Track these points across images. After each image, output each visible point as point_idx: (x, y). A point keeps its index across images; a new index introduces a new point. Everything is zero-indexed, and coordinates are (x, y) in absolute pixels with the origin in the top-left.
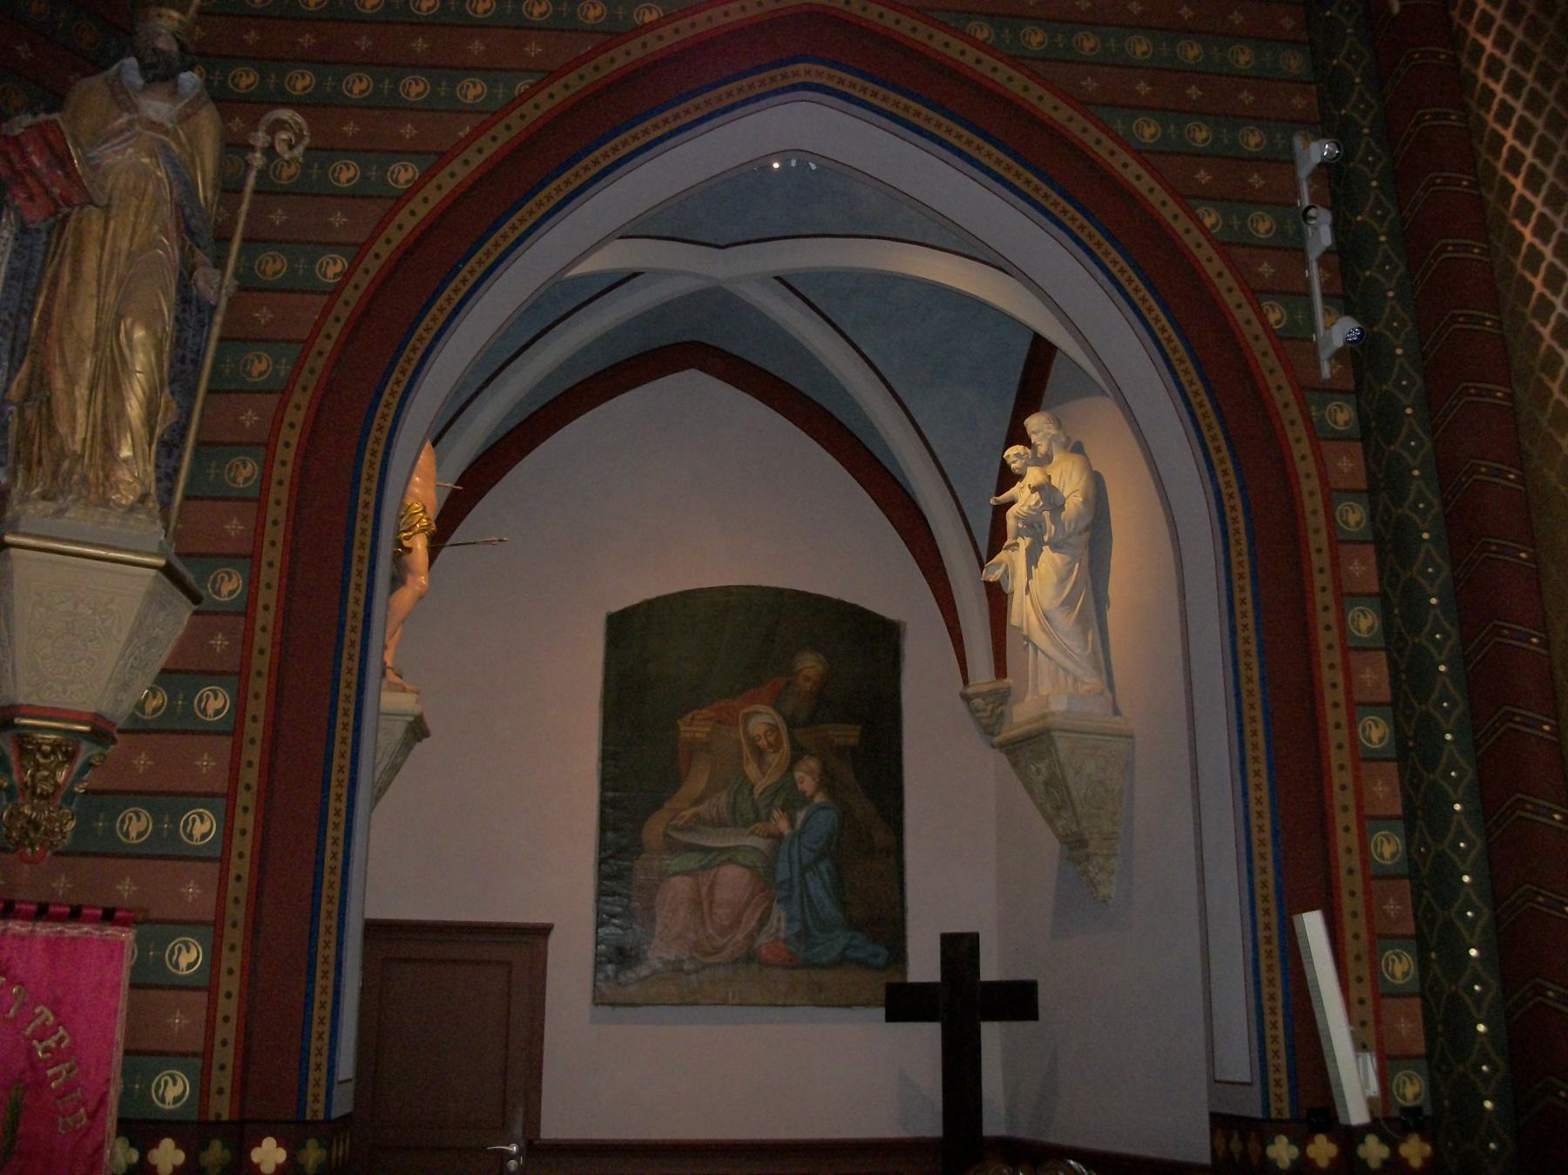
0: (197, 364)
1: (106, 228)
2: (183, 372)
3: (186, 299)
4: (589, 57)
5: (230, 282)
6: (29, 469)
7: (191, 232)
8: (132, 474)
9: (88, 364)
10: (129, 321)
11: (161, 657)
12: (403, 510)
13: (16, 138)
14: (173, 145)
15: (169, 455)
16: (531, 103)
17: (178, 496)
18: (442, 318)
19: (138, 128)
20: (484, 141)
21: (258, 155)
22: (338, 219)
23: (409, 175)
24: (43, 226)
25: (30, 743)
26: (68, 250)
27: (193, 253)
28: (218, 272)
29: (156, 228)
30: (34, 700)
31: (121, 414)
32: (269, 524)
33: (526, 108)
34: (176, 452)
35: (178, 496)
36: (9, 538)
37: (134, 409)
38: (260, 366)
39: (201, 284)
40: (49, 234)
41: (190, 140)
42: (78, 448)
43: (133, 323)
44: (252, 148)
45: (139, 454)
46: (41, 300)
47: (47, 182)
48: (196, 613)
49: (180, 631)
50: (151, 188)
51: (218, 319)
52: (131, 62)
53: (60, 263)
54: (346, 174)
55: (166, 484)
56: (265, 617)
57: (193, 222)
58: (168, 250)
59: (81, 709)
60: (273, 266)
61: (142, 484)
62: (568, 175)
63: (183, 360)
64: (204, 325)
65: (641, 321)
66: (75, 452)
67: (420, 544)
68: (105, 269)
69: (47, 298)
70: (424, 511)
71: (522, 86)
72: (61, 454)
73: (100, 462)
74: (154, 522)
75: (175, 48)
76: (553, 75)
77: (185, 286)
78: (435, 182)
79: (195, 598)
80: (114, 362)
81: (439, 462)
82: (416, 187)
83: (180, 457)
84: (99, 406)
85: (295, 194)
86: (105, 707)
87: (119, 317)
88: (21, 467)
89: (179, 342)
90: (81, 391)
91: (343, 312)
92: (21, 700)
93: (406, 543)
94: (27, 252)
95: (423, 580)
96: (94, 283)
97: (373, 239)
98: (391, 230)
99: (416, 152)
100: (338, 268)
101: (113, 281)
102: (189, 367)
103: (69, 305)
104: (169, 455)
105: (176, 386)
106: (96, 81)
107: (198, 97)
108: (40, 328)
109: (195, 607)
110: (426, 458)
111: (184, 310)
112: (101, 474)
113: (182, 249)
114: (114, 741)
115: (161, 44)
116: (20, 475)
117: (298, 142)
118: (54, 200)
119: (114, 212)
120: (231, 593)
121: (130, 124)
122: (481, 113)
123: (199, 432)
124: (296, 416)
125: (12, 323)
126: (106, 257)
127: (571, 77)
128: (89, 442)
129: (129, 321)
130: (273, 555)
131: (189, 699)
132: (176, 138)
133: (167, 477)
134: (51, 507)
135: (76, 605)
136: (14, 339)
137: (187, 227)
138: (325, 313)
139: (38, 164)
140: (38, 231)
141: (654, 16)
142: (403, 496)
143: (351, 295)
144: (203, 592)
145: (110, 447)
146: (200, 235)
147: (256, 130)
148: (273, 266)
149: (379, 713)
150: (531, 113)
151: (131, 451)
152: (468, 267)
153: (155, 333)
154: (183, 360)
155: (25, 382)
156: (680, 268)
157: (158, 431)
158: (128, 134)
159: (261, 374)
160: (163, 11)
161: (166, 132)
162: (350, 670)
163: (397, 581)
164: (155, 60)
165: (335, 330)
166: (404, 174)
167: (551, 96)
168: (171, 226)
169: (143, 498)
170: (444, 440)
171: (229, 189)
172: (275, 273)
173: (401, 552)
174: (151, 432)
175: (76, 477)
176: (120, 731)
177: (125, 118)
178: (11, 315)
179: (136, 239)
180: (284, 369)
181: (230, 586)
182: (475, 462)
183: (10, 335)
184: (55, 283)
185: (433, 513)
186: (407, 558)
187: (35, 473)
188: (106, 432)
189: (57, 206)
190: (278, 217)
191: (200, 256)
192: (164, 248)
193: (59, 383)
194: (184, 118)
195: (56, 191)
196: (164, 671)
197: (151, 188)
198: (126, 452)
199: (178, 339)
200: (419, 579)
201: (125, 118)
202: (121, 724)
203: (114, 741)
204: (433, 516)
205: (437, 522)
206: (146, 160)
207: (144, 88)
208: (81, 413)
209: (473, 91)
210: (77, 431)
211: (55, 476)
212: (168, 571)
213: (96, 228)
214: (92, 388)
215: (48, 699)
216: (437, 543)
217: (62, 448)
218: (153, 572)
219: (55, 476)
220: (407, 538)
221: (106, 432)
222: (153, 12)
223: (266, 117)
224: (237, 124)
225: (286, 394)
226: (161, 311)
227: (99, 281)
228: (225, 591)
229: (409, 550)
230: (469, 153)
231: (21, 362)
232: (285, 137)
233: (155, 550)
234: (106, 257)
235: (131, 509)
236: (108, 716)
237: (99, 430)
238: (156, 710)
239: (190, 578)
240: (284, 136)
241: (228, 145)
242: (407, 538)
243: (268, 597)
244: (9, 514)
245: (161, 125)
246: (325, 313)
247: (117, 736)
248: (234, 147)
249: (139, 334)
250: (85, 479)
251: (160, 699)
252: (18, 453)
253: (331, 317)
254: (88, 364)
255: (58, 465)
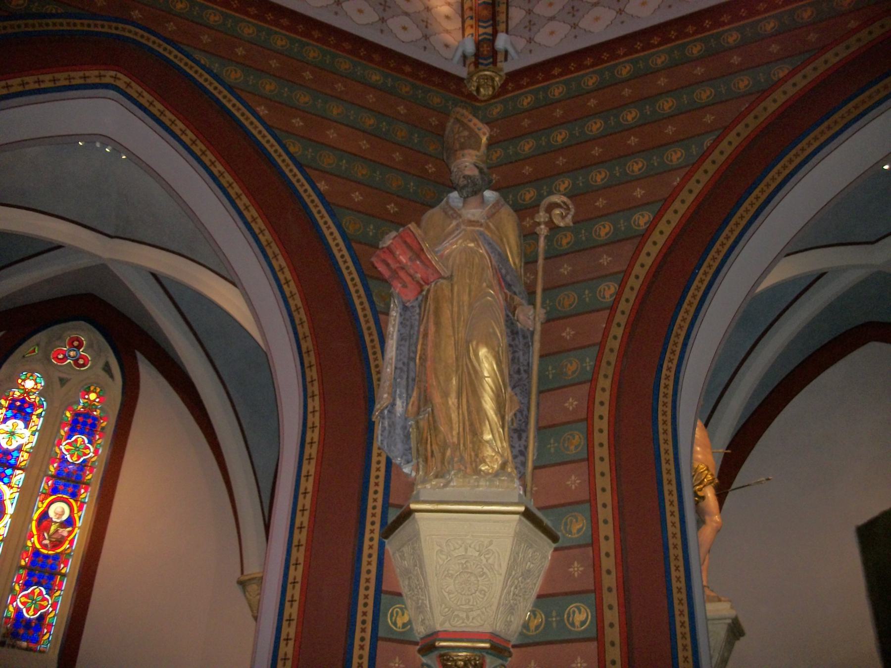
0: (528, 372)
1: (452, 290)
2: (520, 380)
3: (513, 330)
4: (749, 110)
5: (541, 313)
6: (426, 460)
7: (509, 286)
8: (494, 450)
9: (454, 382)
10: (474, 343)
11: (535, 586)
12: (694, 471)
13: (388, 248)
14: (487, 232)
15: (520, 438)
16: (717, 152)
17: (530, 465)
18: (692, 310)
19: (463, 227)
20: (692, 184)
21: (543, 227)
22: (605, 260)
23: (646, 219)
24: (416, 304)
25: (448, 660)
26: (431, 312)
27: (512, 299)
28: (531, 307)
29: (484, 285)
30: (447, 627)
31: (480, 409)
32: (598, 476)
33: (715, 155)
34: (524, 435)
35: (530, 465)
36: (413, 506)
37: (489, 405)
38: (572, 367)
39: (521, 317)
40: (420, 307)
41: (498, 229)
42: (455, 440)
43: (477, 345)
44: (539, 224)
45: (497, 436)
46: (419, 347)
47: (412, 272)
48: (556, 550)
49: (547, 564)
50: (477, 260)
51: (537, 337)
52: (455, 195)
53: (427, 322)
54: (604, 230)
55: (521, 458)
56: (607, 546)
57: (508, 278)
58: (494, 295)
59: (481, 630)
60: (568, 300)
61: (502, 456)
62: (756, 192)
63: (519, 372)
64: (528, 346)
65: (832, 309)
66: (454, 443)
67: (710, 493)
68: (456, 316)
69: (423, 344)
70: (708, 469)
71: (708, 142)
72: (444, 446)
73: (471, 446)
74: (512, 481)
75: (476, 172)
76: (727, 129)
77: (512, 324)
78: (664, 219)
79: (554, 538)
80: (469, 373)
81: (711, 437)
82: (652, 225)
83: (527, 440)
84: (465, 407)
85: (572, 252)
86: (499, 627)
87: (468, 343)
88: (421, 460)
89: (514, 360)
90: (452, 401)
91: (621, 318)
92: (438, 628)
93: (699, 493)
94: (408, 323)
95: (717, 518)
96: (451, 328)
97: (631, 266)
98: (643, 258)
99: (648, 204)
100: (613, 290)
101: (462, 324)
102: (524, 376)
103: (437, 346)
104: (520, 438)
105: (517, 390)
106: (437, 209)
107: (469, 82)
108: (421, 364)
109: (554, 545)
110: (700, 432)
111: (514, 339)
112: (473, 454)
113: (506, 300)
114: (510, 655)
115: (467, 172)
116: (421, 466)
117: (567, 214)
118: (418, 283)
119: (455, 279)
120: (579, 531)
121: (458, 225)
122: (685, 166)
123: (537, 422)
124: (603, 396)
125: (405, 369)
126: (455, 309)
127: (740, 128)
128: (461, 433)
129: (474, 343)
130: (605, 498)
131: (560, 615)
132: (488, 227)
133: (520, 454)
134: (441, 482)
135: (466, 550)
136: (408, 378)
137: (505, 281)
138: (610, 321)
139: (404, 261)
140: (413, 307)
141: (787, 72)
142: (691, 463)
143: (625, 306)
144: (559, 534)
145: (476, 433)
146: (516, 287)
147: (538, 212)
148: (568, 300)
149: (707, 620)
150: (719, 157)
151: (493, 440)
152: (702, 271)
153: (493, 349)
154: (519, 372)
155: (416, 403)
156: (849, 265)
157: (508, 418)
158: (457, 232)
159: (574, 372)
160: (466, 152)
161: (481, 225)
162: (673, 524)
163: (701, 522)
164: (465, 182)
165: (618, 332)
166: (642, 219)
167: (730, 143)
168: (495, 283)
169: (503, 466)
170: (712, 421)
171: (530, 261)
172: (570, 305)
173: (699, 499)
174: (502, 418)
175: (456, 459)
176: (514, 646)
177: (454, 223)
178: (404, 364)
179: (473, 293)
180: (589, 364)
181: (576, 527)
182: (736, 435)
183: (405, 377)
184: (426, 335)
185: (715, 471)
186: (702, 504)
187: (430, 463)
188: (472, 424)
189: (421, 286)
190: (566, 270)
191: (517, 299)
192: (491, 295)
193: (437, 399)
194: (491, 216)
195: (419, 276)
196: (539, 597)
197: (477, 260)
198: (488, 437)
199: (513, 359)
200: (715, 518)
201: (454, 223)
202: (514, 641)
203: (510, 655)
204: (716, 475)
205: (719, 477)
206: (472, 245)
207: (464, 206)
208: (454, 416)
209: (675, 156)
210: (452, 427)
211: (443, 463)
212: (528, 514)
213: (447, 292)
214: (459, 396)
215: (457, 625)
216: (721, 497)
217: (445, 441)
218: (517, 517)
219: (443, 463)
220: (701, 490)
221: (472, 424)
222: (459, 153)
223: (543, 202)
224: (528, 223)
225: (593, 381)
226: (495, 334)
227: (453, 327)
228: (574, 531)
229: (703, 498)
230: (684, 194)
231: (413, 389)
232: (558, 210)
233: (516, 500)
234: (455, 309)
235: (496, 475)
236: (503, 635)
237: (467, 423)
238: (537, 627)
239: (547, 522)
240: (557, 211)
241: (524, 236)
242: (701, 490)
243: (606, 530)
244: (415, 492)
245: (478, 222)
246: (610, 321)
247: (512, 650)
248: (528, 236)
249: (483, 352)
250: (462, 458)
251: (540, 619)
252: (418, 450)
253: (614, 324)
254: (454, 382)
255: (444, 454)
